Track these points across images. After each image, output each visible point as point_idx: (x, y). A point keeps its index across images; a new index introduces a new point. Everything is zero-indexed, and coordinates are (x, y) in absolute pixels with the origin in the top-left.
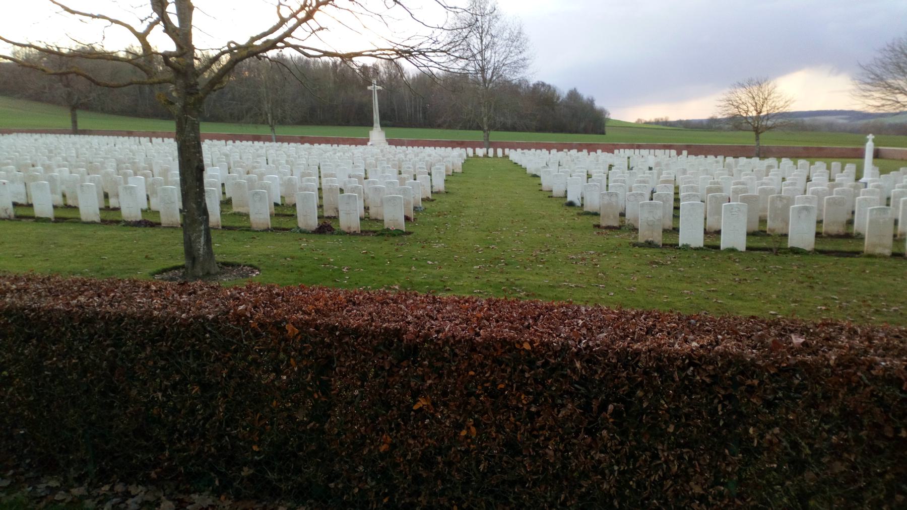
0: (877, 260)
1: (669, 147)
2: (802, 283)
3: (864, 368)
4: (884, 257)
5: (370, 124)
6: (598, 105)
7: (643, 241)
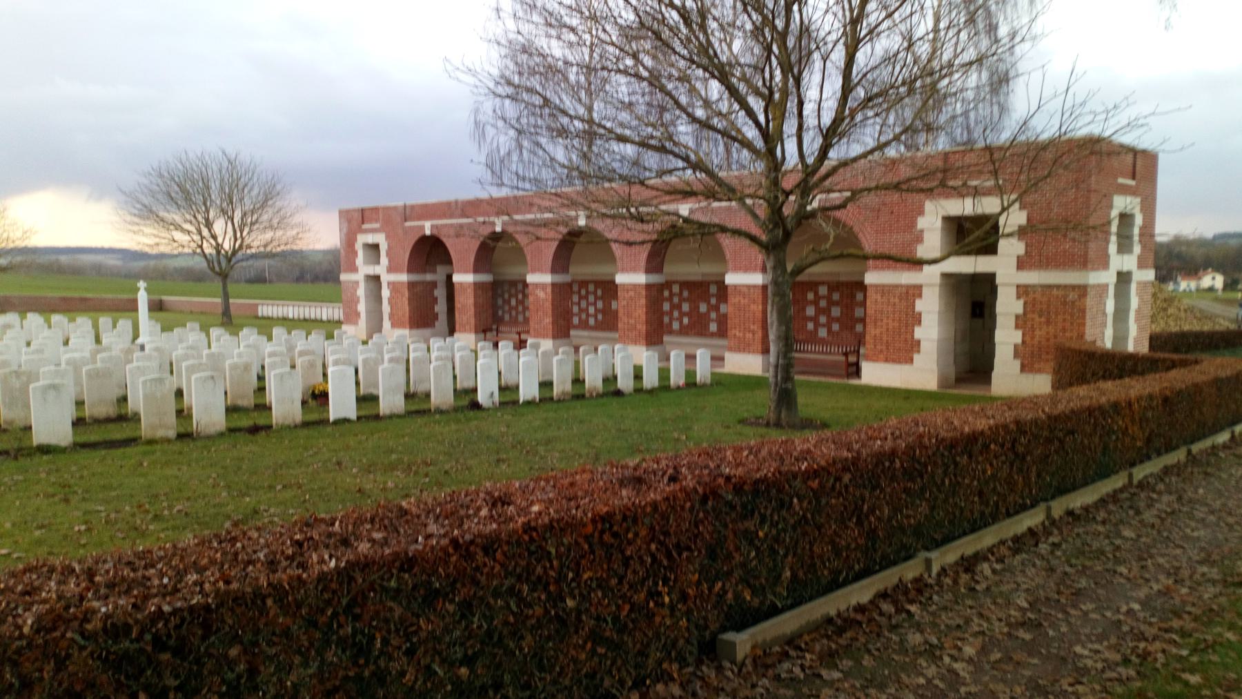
0: (158, 447)
2: (53, 496)
3: (76, 624)
4: (168, 441)
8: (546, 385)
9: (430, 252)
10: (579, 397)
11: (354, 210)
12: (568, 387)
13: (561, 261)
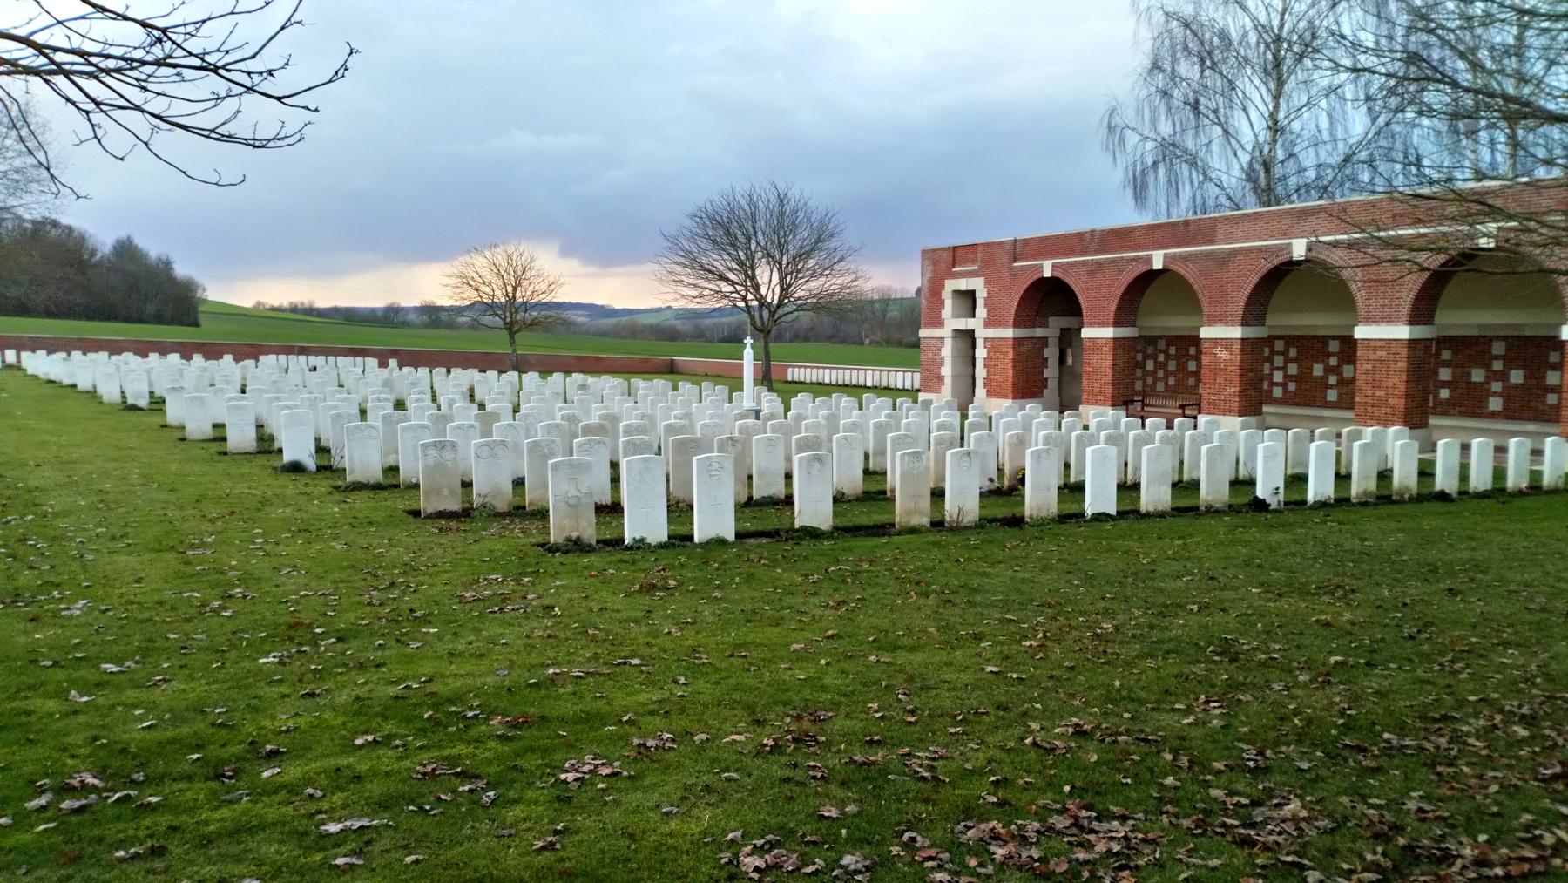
6: (181, 270)
7: (560, 540)
8: (1128, 489)
9: (1050, 300)
10: (1342, 502)
11: (944, 249)
12: (1372, 485)
13: (1255, 310)
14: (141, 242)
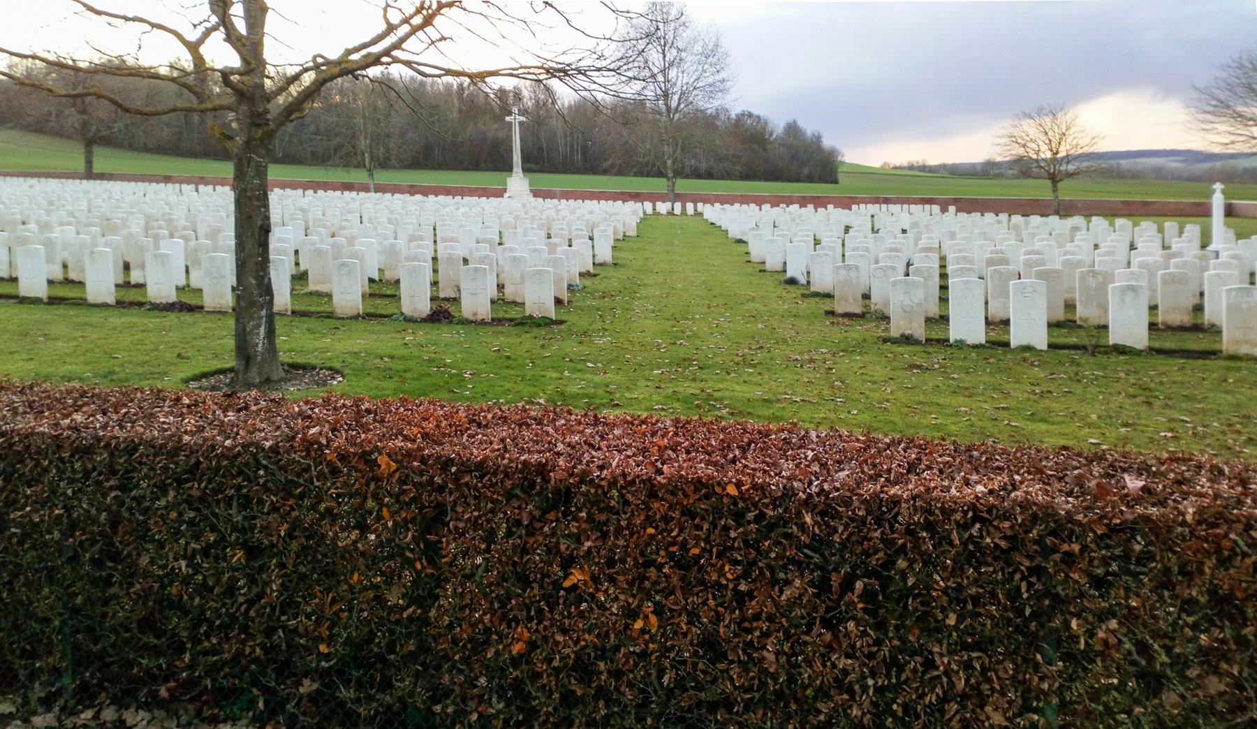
1: (930, 201)
2: (1135, 396)
3: (1240, 527)
5: (509, 168)
6: (827, 143)
14: (802, 124)
